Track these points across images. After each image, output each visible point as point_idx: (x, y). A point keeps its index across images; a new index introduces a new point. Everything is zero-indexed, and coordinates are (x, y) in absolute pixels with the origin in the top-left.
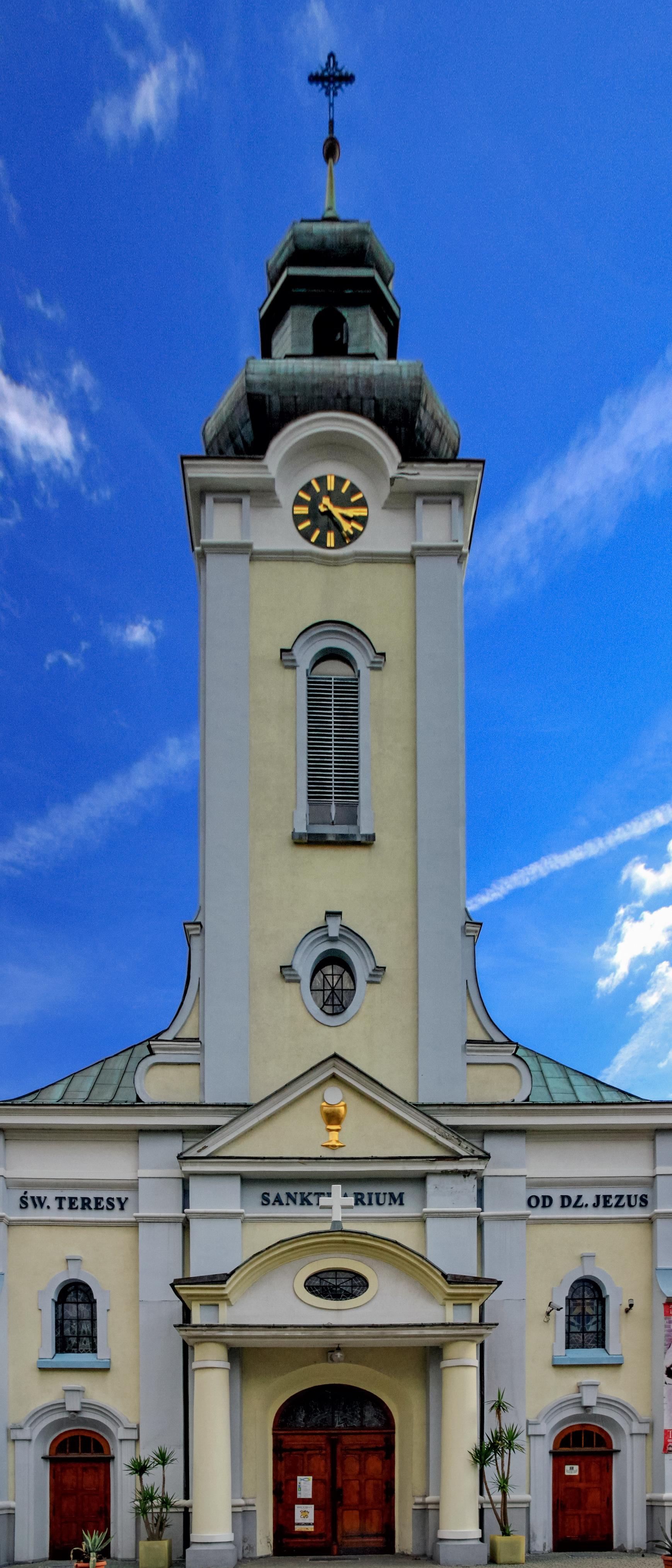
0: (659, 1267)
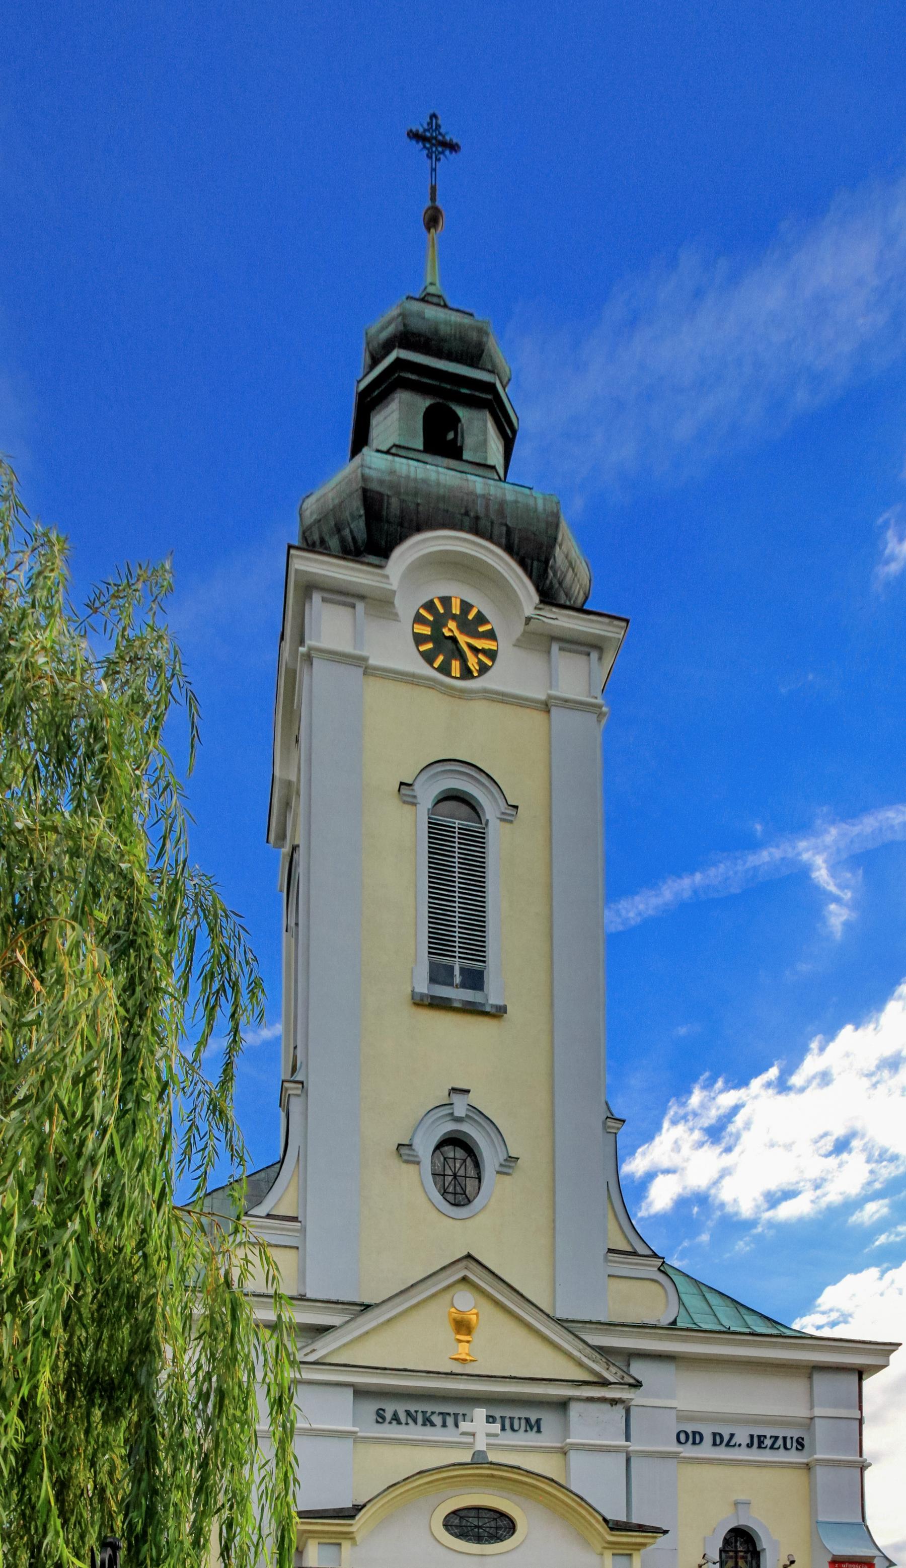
0: (820, 1519)
